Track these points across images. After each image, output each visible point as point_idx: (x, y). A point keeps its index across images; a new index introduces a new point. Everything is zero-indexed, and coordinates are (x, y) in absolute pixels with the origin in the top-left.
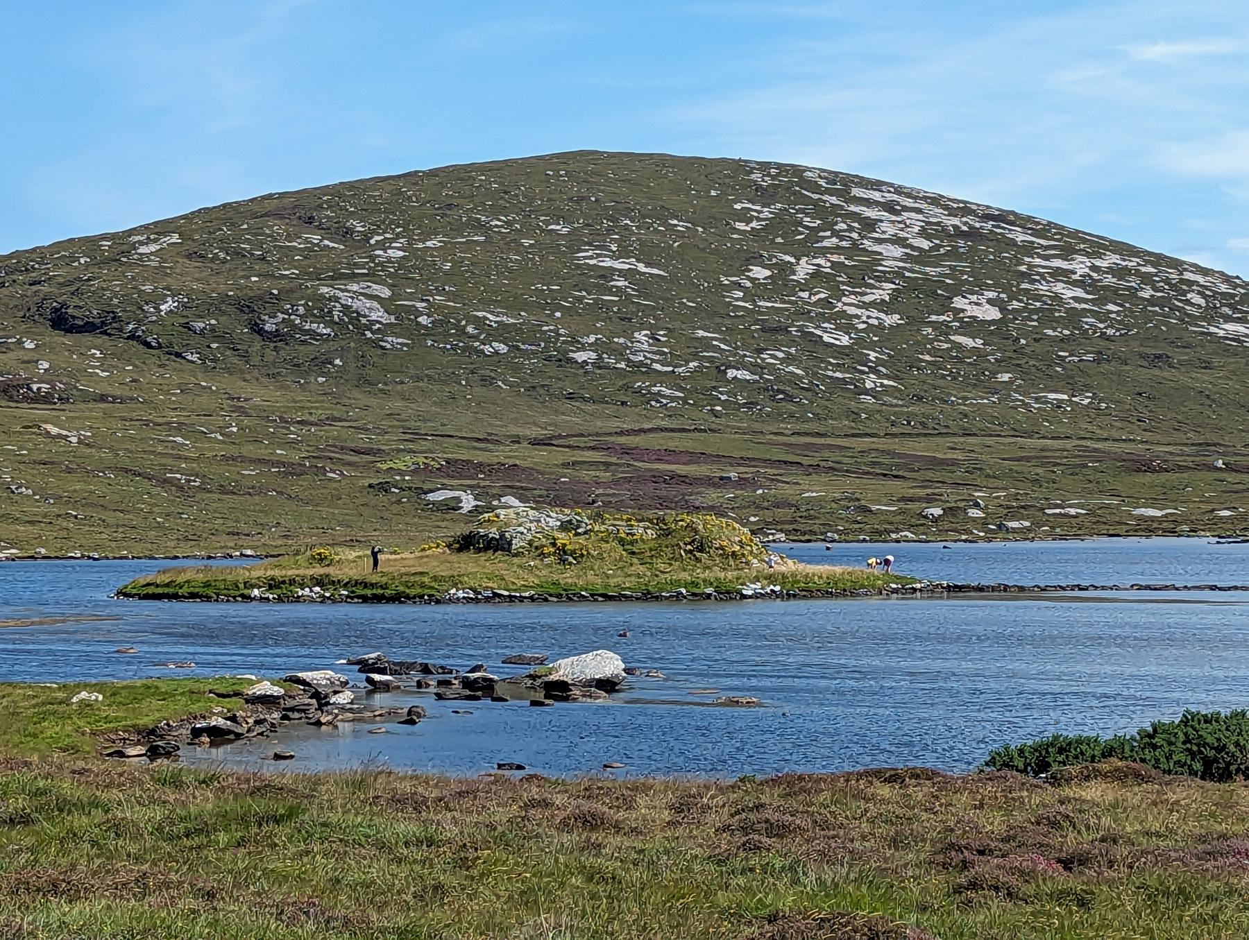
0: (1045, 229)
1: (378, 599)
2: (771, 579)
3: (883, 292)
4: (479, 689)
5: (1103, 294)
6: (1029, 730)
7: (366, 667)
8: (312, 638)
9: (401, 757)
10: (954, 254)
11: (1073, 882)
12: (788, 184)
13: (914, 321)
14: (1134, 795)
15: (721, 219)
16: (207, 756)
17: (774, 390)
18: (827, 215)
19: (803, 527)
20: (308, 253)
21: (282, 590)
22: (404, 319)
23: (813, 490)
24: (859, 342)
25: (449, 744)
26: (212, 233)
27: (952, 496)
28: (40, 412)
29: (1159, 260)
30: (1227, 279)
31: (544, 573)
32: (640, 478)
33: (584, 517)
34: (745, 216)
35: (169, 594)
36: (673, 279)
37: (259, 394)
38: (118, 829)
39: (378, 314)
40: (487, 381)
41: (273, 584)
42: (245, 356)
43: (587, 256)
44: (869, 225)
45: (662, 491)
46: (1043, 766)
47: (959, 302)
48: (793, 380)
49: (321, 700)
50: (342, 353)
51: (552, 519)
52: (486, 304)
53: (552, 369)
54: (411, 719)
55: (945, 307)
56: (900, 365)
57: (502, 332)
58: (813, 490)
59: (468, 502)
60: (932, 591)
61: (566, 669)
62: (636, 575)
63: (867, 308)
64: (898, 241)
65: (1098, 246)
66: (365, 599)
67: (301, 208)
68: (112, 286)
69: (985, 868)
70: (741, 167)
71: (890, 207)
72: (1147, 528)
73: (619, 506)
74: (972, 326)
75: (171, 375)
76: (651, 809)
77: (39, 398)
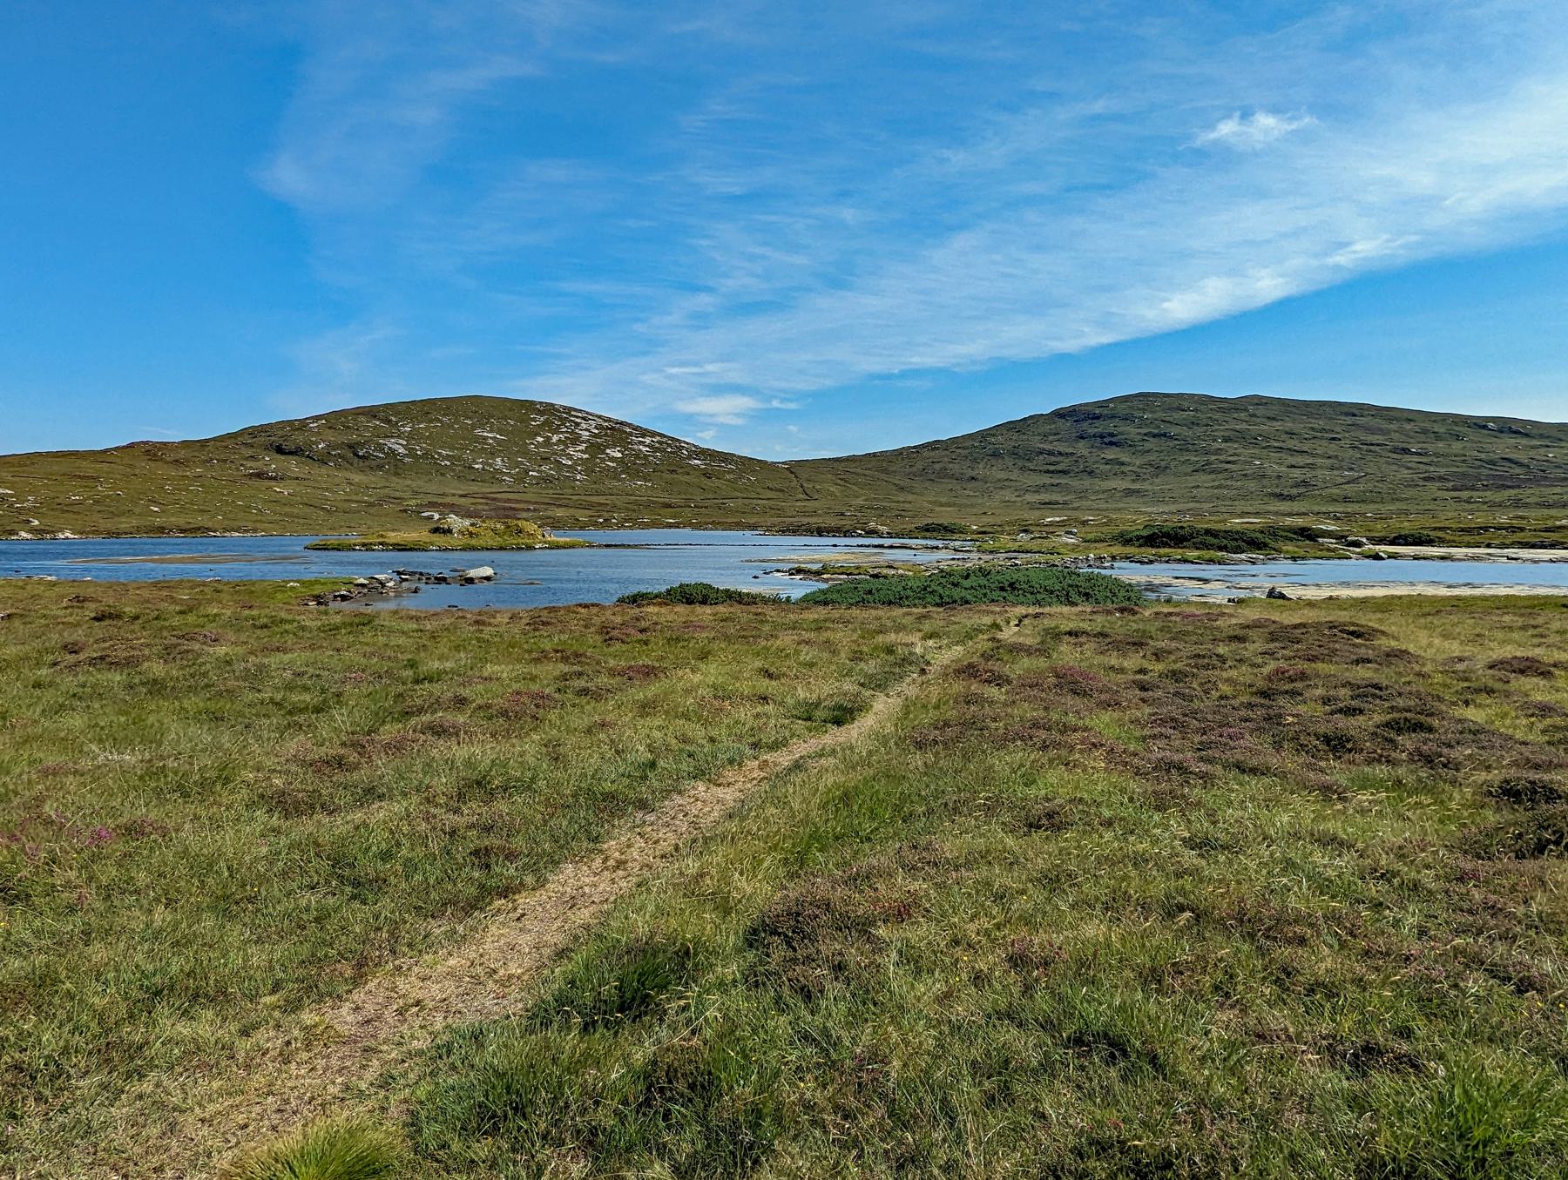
0: (636, 428)
3: (583, 447)
4: (441, 580)
5: (656, 450)
6: (634, 590)
7: (399, 573)
8: (382, 565)
9: (410, 604)
11: (643, 637)
12: (549, 409)
13: (593, 457)
14: (663, 610)
15: (525, 420)
16: (339, 605)
17: (547, 480)
19: (556, 525)
20: (375, 427)
21: (367, 547)
22: (411, 453)
23: (560, 513)
25: (432, 598)
26: (334, 420)
27: (606, 515)
28: (273, 483)
29: (672, 439)
31: (466, 540)
32: (499, 508)
33: (479, 521)
35: (324, 548)
37: (357, 478)
38: (303, 628)
41: (364, 545)
43: (478, 432)
44: (578, 424)
45: (507, 513)
46: (634, 601)
49: (383, 585)
51: (467, 522)
54: (416, 591)
55: (603, 452)
56: (589, 471)
57: (448, 457)
58: (560, 513)
59: (437, 516)
60: (600, 546)
61: (472, 573)
62: (498, 541)
65: (654, 434)
67: (371, 412)
68: (300, 439)
69: (615, 633)
70: (532, 403)
72: (670, 526)
73: (491, 518)
74: (613, 459)
75: (323, 470)
76: (502, 619)
77: (271, 478)
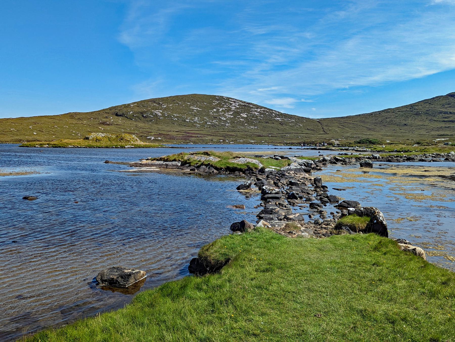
1: (56, 147)
2: (132, 145)
3: (231, 113)
10: (242, 108)
12: (221, 98)
13: (235, 117)
17: (214, 126)
18: (225, 102)
22: (163, 115)
24: (227, 119)
30: (278, 112)
34: (214, 103)
36: (203, 111)
37: (140, 125)
39: (160, 114)
40: (173, 124)
42: (141, 120)
43: (192, 107)
44: (231, 104)
47: (241, 114)
48: (216, 124)
50: (154, 119)
52: (176, 113)
53: (183, 122)
55: (239, 115)
57: (177, 117)
63: (229, 115)
64: (234, 106)
65: (262, 107)
66: (54, 147)
71: (234, 102)
74: (243, 118)
